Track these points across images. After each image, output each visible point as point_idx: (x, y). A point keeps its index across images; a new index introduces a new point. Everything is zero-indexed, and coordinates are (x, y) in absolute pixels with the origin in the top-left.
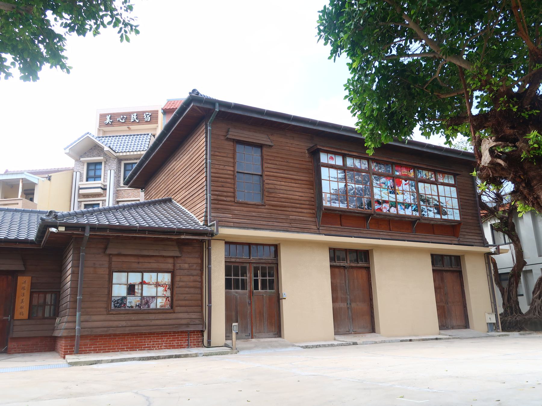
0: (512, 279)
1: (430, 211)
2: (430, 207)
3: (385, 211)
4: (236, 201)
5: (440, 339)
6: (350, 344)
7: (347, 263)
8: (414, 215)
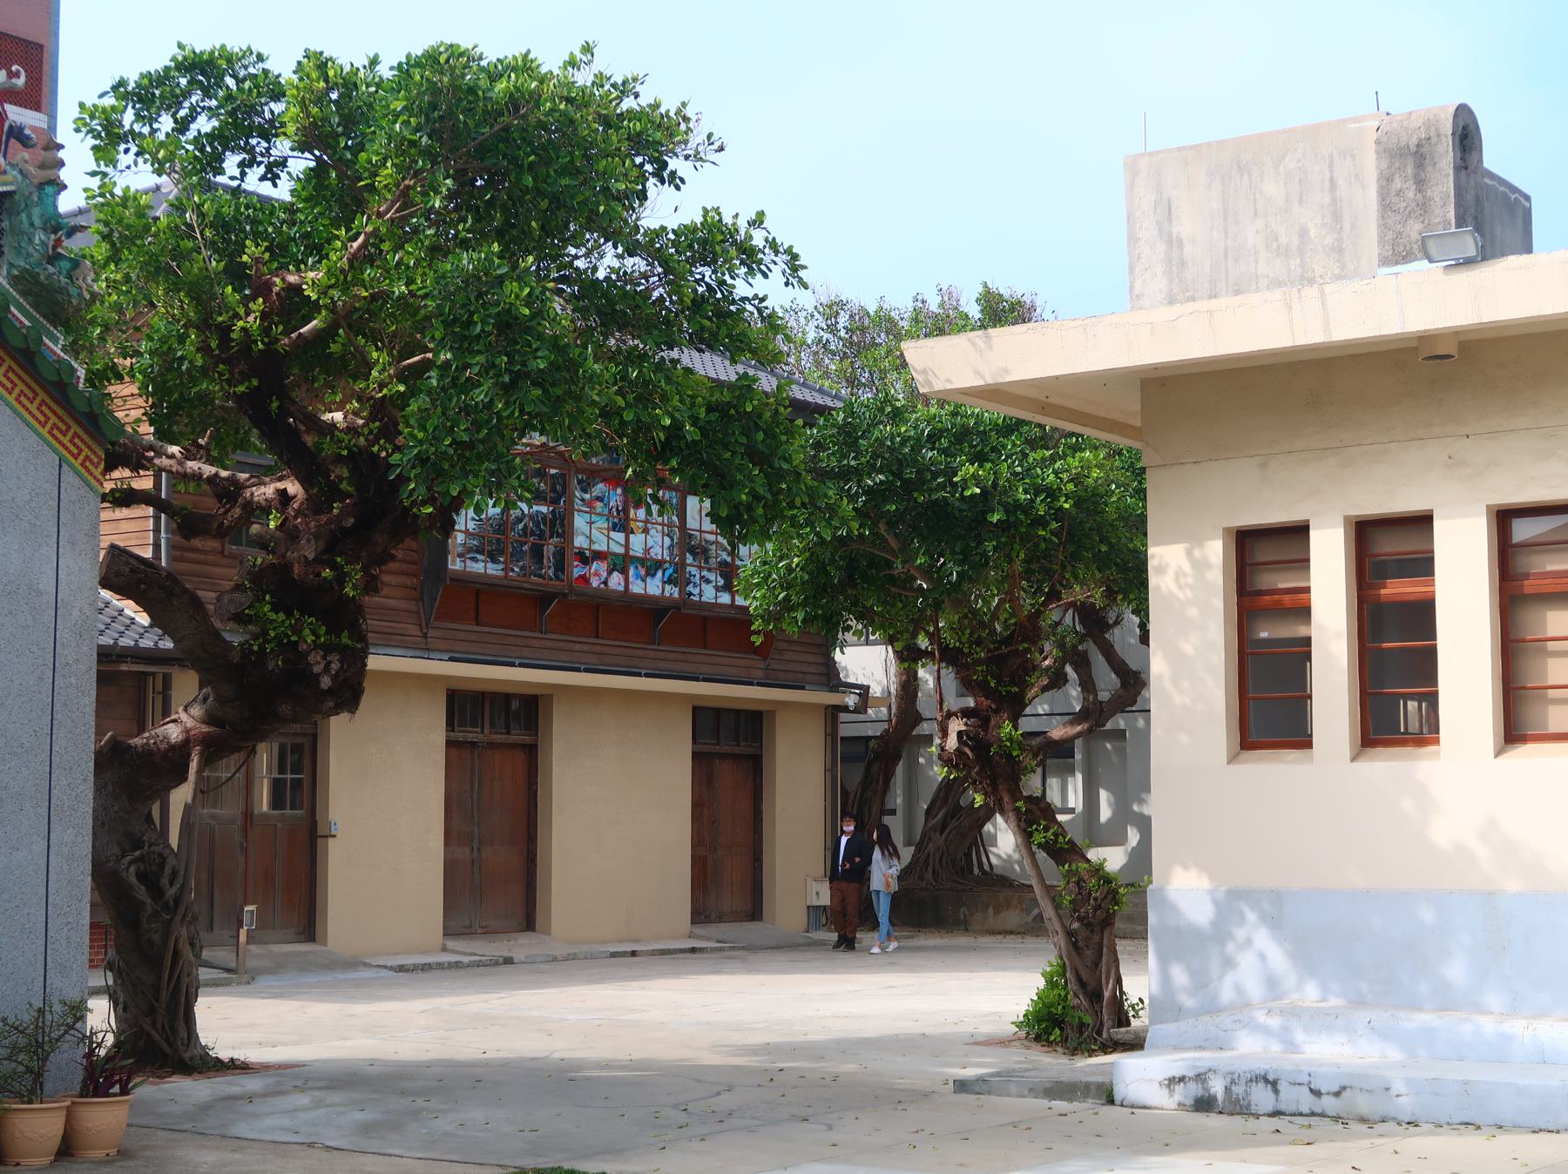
0: (876, 767)
1: (708, 581)
2: (709, 570)
4: (226, 553)
5: (701, 950)
6: (496, 963)
7: (482, 732)
8: (668, 595)
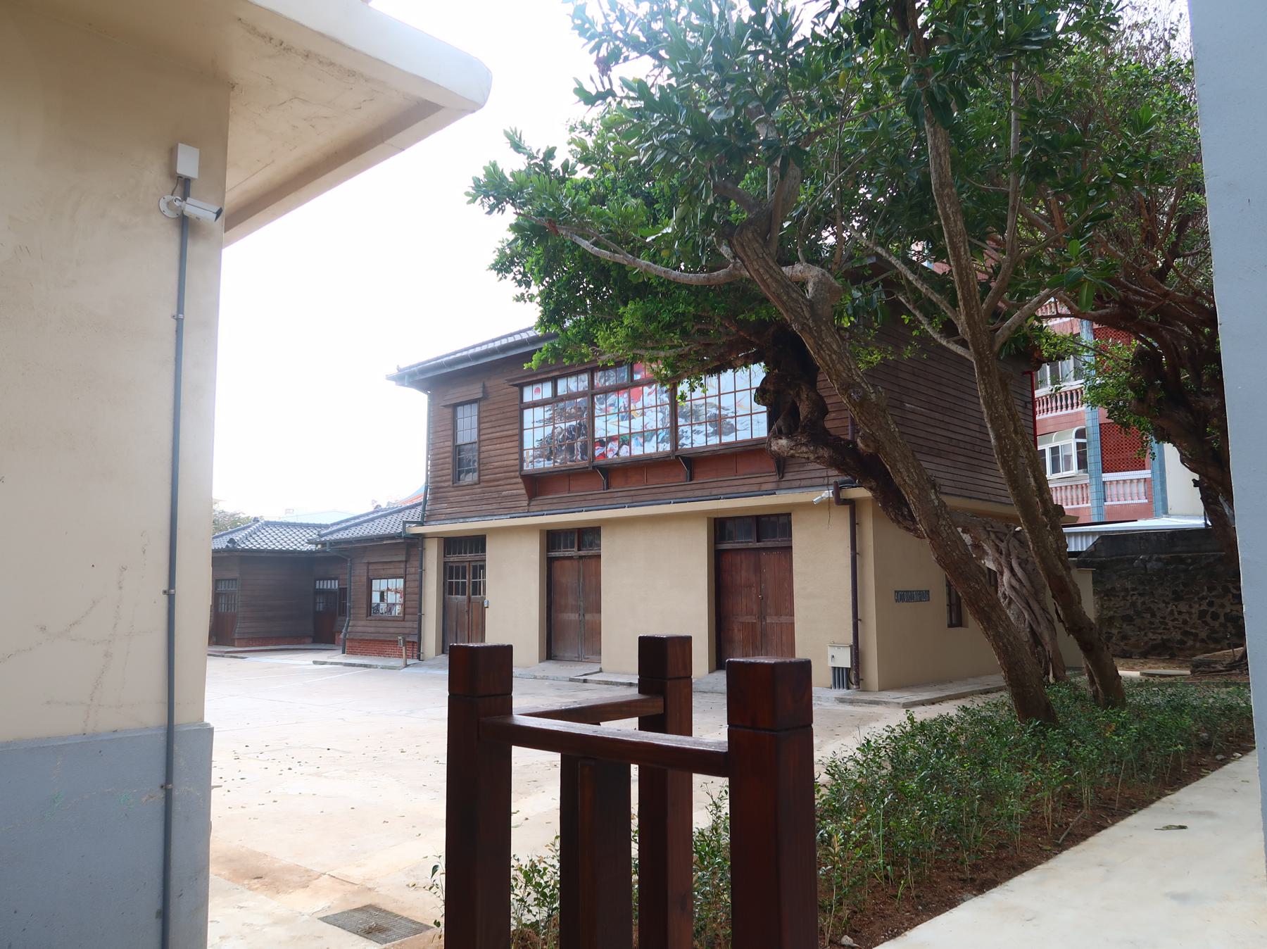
3: (610, 455)
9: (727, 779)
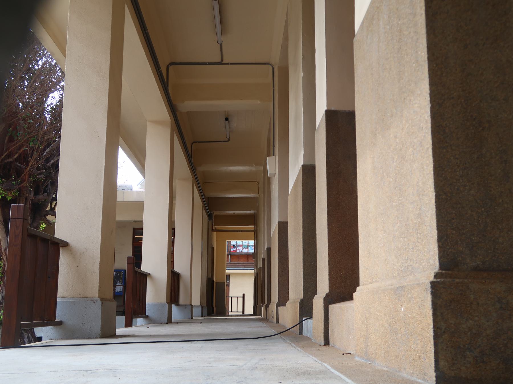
3: (238, 251)
9: (253, 314)
